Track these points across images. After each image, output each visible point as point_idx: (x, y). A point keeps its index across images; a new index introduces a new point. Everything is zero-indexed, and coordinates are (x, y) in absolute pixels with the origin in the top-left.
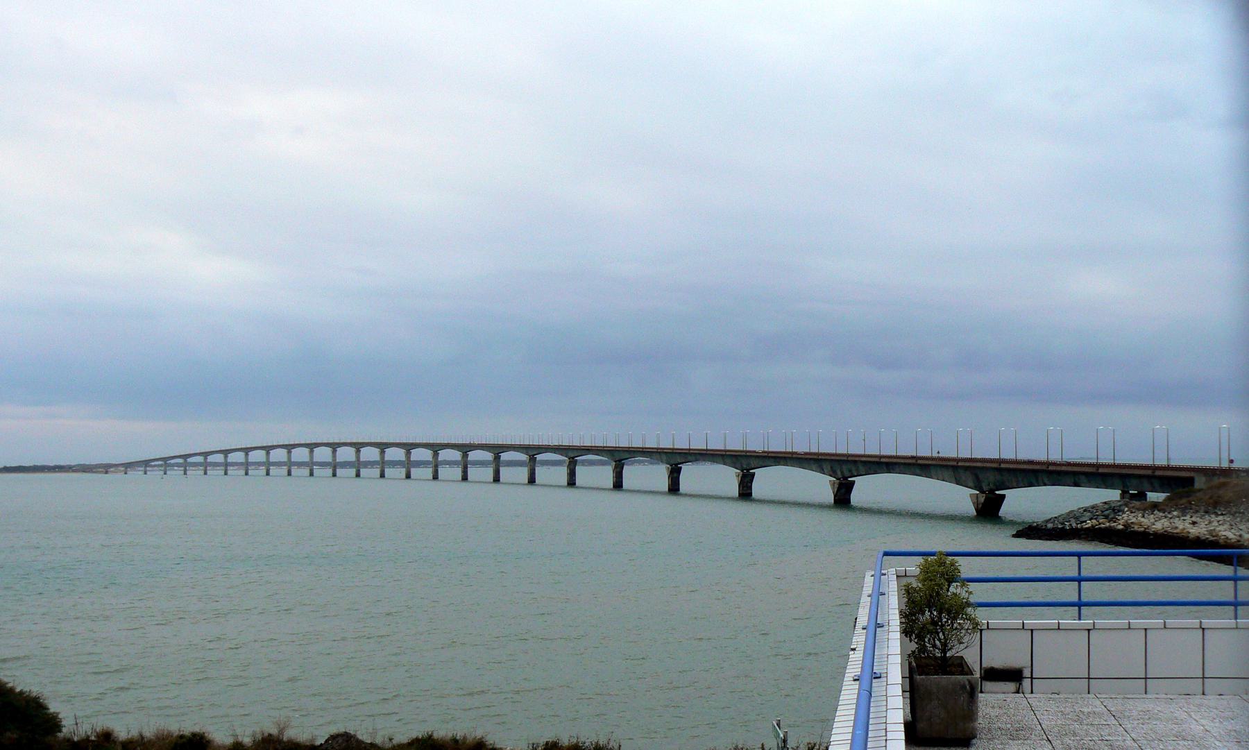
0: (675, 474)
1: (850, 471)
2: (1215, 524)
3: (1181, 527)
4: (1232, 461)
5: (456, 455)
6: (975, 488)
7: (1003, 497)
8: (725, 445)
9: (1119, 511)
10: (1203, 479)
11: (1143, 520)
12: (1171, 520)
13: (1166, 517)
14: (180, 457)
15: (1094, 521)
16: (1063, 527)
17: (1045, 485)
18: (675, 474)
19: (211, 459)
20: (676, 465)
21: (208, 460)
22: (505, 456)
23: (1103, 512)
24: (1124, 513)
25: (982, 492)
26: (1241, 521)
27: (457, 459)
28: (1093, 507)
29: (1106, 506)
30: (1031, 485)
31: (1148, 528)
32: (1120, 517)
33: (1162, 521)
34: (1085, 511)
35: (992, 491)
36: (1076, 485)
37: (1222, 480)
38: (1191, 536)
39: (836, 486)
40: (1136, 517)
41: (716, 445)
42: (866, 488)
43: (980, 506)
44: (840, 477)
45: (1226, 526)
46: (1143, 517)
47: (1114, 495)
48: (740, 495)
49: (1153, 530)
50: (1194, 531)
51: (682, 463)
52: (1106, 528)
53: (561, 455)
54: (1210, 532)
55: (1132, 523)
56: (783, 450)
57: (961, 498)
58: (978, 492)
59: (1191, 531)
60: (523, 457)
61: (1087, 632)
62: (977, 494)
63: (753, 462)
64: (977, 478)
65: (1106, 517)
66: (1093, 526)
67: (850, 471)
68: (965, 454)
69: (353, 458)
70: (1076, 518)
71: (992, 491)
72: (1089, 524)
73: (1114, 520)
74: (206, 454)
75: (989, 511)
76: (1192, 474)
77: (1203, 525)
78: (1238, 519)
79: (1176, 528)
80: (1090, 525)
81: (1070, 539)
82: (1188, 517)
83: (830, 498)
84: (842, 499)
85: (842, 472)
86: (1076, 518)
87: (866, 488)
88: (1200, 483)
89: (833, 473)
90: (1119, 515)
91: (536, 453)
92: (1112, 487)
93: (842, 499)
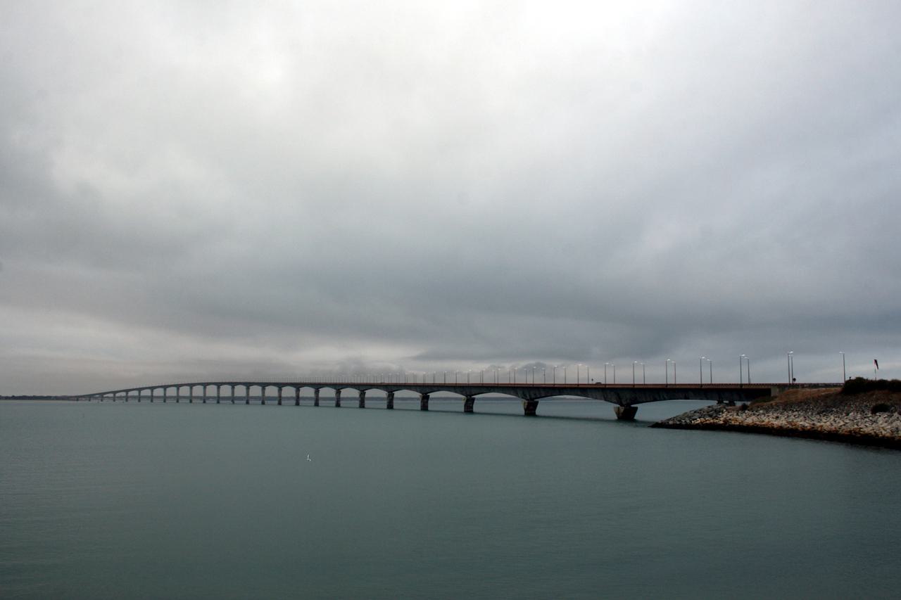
0: (425, 399)
2: (792, 417)
3: (767, 420)
4: (794, 380)
5: (355, 393)
7: (636, 408)
8: (434, 380)
9: (720, 412)
10: (778, 390)
12: (759, 417)
13: (754, 414)
14: (727, 427)
15: (702, 419)
17: (665, 399)
18: (425, 399)
19: (130, 394)
20: (426, 394)
22: (397, 394)
23: (708, 412)
24: (723, 413)
25: (621, 405)
26: (812, 414)
28: (700, 410)
29: (710, 409)
30: (655, 400)
33: (752, 418)
35: (629, 405)
37: (795, 390)
38: (775, 426)
40: (733, 415)
42: (646, 411)
43: (620, 415)
45: (802, 418)
46: (737, 415)
47: (714, 403)
48: (525, 414)
50: (777, 423)
52: (711, 423)
53: (456, 392)
54: (790, 423)
56: (587, 383)
57: (609, 410)
59: (774, 423)
60: (417, 395)
63: (474, 391)
64: (618, 395)
65: (711, 416)
66: (701, 422)
69: (162, 394)
70: (690, 417)
71: (629, 405)
72: (699, 421)
73: (716, 418)
74: (127, 391)
75: (627, 416)
76: (769, 387)
77: (783, 418)
78: (810, 413)
79: (763, 421)
81: (806, 438)
82: (771, 414)
83: (462, 409)
84: (469, 409)
85: (530, 396)
86: (690, 417)
87: (543, 407)
88: (774, 392)
89: (524, 397)
92: (712, 399)
93: (469, 409)
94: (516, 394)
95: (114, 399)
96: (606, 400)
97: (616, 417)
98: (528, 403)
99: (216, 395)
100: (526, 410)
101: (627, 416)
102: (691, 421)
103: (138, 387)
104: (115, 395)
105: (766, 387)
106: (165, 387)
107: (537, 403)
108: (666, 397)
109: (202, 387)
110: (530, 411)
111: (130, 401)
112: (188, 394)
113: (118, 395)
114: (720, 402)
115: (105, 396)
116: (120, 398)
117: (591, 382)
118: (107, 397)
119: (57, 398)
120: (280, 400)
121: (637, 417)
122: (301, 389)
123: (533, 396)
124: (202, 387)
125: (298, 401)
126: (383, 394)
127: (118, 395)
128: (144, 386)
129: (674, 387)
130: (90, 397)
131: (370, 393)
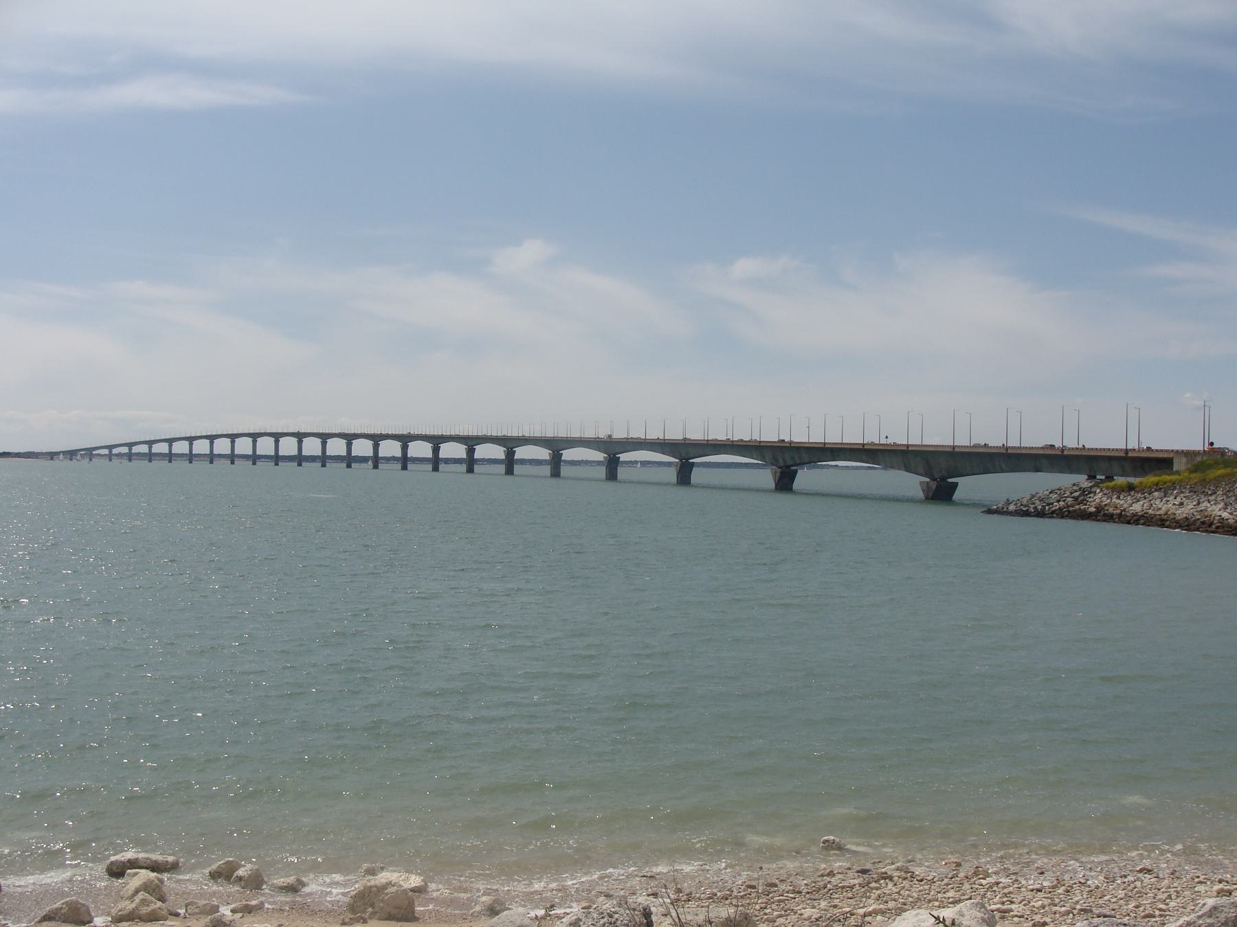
1: (792, 458)
3: (1164, 509)
4: (1212, 444)
5: (498, 452)
6: (925, 475)
8: (684, 432)
9: (1090, 493)
11: (1118, 501)
14: (1102, 515)
16: (1028, 510)
17: (1002, 471)
19: (135, 449)
20: (614, 455)
21: (133, 451)
22: (567, 455)
27: (462, 457)
30: (986, 471)
31: (1124, 510)
32: (1092, 499)
33: (1142, 503)
34: (1051, 493)
36: (1037, 470)
39: (778, 474)
41: (103, 445)
42: (968, 486)
43: (931, 494)
44: (782, 465)
46: (1118, 498)
49: (1132, 512)
50: (1181, 513)
51: (517, 447)
55: (1106, 505)
57: (912, 483)
58: (928, 480)
60: (599, 456)
61: (272, 440)
62: (928, 482)
67: (792, 458)
68: (915, 440)
71: (943, 479)
74: (130, 445)
75: (941, 493)
80: (1057, 507)
87: (805, 478)
89: (774, 462)
90: (1090, 497)
91: (474, 444)
92: (1078, 471)
94: (762, 458)
95: (110, 457)
96: (907, 471)
97: (921, 495)
98: (782, 473)
99: (250, 453)
100: (776, 485)
101: (941, 493)
102: (1044, 507)
103: (148, 439)
104: (130, 450)
105: (1166, 455)
106: (191, 440)
107: (796, 472)
108: (1003, 466)
109: (187, 443)
110: (785, 482)
111: (218, 463)
112: (318, 452)
113: (115, 451)
114: (1091, 477)
115: (94, 452)
116: (120, 455)
117: (883, 441)
118: (99, 455)
119: (18, 455)
120: (376, 460)
121: (957, 495)
122: (195, 443)
123: (789, 462)
124: (187, 443)
125: (436, 462)
126: (544, 454)
127: (115, 451)
128: (199, 434)
129: (1018, 452)
130: (71, 454)
131: (521, 453)
